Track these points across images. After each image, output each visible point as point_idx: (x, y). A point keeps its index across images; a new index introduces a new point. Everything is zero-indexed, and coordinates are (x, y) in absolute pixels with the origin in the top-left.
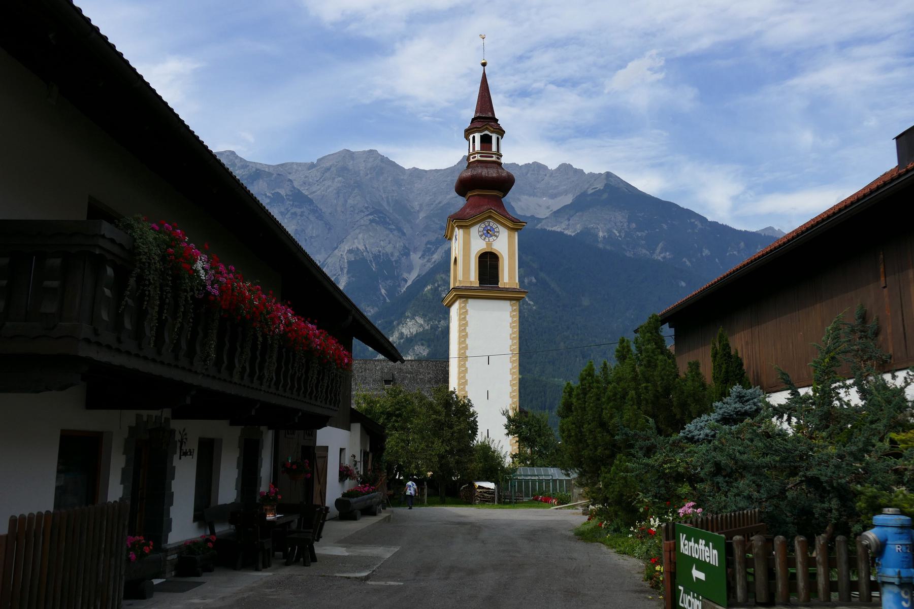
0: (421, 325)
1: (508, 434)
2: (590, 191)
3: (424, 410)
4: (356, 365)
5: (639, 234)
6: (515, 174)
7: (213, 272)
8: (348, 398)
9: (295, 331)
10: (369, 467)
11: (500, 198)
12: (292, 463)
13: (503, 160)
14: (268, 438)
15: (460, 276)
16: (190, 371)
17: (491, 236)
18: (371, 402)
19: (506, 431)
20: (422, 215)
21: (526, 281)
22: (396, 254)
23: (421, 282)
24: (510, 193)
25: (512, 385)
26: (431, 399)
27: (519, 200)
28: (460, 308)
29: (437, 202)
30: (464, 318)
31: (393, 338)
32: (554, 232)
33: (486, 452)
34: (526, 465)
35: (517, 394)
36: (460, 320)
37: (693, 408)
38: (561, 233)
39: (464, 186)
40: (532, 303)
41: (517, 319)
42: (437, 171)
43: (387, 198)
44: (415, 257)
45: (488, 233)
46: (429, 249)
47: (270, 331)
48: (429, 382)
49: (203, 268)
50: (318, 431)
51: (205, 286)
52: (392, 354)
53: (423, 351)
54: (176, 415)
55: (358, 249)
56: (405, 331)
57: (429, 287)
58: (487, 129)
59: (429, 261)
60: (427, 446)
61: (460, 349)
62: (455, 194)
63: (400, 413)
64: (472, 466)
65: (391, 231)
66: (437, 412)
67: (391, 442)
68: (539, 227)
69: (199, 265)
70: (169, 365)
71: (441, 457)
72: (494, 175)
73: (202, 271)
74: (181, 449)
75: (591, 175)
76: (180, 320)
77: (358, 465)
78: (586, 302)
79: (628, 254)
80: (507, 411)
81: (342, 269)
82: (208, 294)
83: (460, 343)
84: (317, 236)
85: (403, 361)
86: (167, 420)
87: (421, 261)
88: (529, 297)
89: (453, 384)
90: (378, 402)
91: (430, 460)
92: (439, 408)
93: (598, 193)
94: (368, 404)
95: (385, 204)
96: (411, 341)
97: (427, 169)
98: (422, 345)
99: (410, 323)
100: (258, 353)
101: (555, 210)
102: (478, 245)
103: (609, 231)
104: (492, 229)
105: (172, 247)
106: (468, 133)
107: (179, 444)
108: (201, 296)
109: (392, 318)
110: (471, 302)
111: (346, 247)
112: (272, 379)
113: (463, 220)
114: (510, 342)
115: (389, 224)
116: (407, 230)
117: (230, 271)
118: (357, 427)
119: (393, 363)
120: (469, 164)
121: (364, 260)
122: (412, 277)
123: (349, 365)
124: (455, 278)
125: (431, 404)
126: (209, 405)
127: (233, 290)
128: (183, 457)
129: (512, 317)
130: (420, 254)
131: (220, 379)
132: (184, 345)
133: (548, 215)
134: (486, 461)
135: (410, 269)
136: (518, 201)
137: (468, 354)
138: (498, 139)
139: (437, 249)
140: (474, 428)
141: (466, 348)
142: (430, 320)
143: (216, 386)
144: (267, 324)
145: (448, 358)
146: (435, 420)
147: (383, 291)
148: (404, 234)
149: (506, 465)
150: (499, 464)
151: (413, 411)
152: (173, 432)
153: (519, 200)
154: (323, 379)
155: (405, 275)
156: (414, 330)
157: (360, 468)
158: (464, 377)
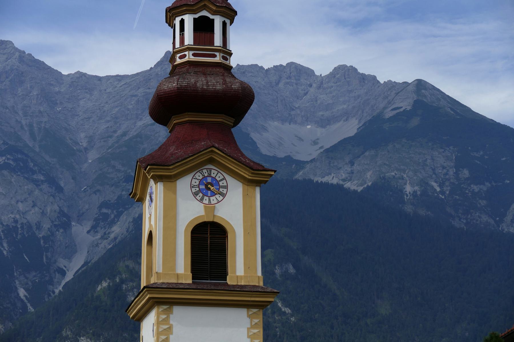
2: (389, 114)
5: (476, 188)
6: (255, 83)
11: (230, 127)
13: (233, 62)
15: (158, 266)
17: (214, 194)
20: (92, 156)
22: (46, 225)
23: (90, 274)
24: (248, 118)
27: (265, 129)
28: (159, 323)
29: (119, 132)
32: (327, 185)
38: (339, 187)
39: (166, 106)
40: (288, 311)
42: (119, 78)
43: (31, 126)
44: (80, 231)
45: (208, 189)
57: (105, 284)
58: (205, 8)
59: (104, 237)
62: (148, 120)
65: (37, 183)
68: (300, 176)
72: (219, 87)
75: (391, 85)
78: (384, 309)
79: (457, 224)
87: (90, 238)
88: (284, 301)
93: (403, 116)
95: (26, 137)
97: (102, 73)
101: (327, 146)
102: (191, 210)
103: (424, 183)
104: (215, 182)
106: (171, 14)
110: (178, 311)
113: (163, 166)
115: (34, 172)
116: (66, 181)
120: (175, 67)
122: (74, 267)
133: (315, 155)
135: (71, 251)
136: (263, 133)
138: (224, 24)
139: (118, 216)
147: (22, 293)
148: (60, 190)
153: (265, 129)
155: (62, 263)
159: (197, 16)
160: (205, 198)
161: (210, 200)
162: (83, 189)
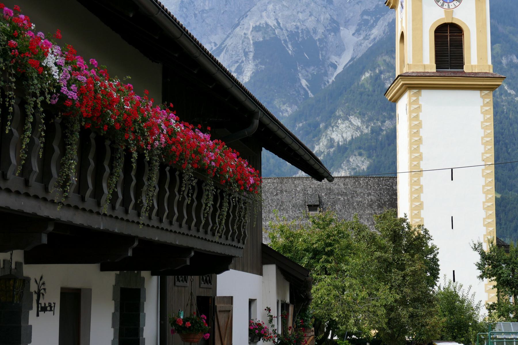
0: (358, 128)
1: (481, 277)
3: (364, 245)
4: (267, 185)
7: (69, 68)
8: (258, 231)
9: (182, 143)
10: (290, 323)
12: (185, 320)
14: (152, 286)
15: (409, 59)
16: (45, 199)
18: (291, 237)
19: (479, 273)
21: (504, 61)
22: (321, 30)
23: (356, 67)
25: (486, 209)
26: (373, 230)
28: (410, 103)
30: (417, 117)
31: (319, 148)
33: (452, 302)
34: (508, 319)
35: (493, 220)
36: (411, 119)
37: (445, 339)
40: (513, 92)
41: (490, 116)
44: (347, 34)
46: (367, 21)
47: (147, 143)
48: (371, 206)
49: (56, 64)
50: (218, 276)
51: (59, 88)
52: (316, 170)
53: (361, 163)
54: (30, 259)
55: (267, 24)
56: (336, 137)
57: (367, 75)
60: (370, 294)
61: (411, 160)
63: (329, 251)
64: (432, 321)
66: (382, 248)
67: (320, 290)
69: (50, 61)
70: (18, 193)
71: (390, 309)
73: (55, 69)
74: (38, 303)
76: (29, 133)
77: (275, 321)
80: (480, 245)
81: (246, 54)
82: (63, 98)
83: (411, 152)
84: (211, 9)
85: (331, 179)
86: (19, 265)
87: (355, 39)
88: (509, 84)
89: (404, 208)
90: (301, 235)
91: (374, 312)
92: (384, 242)
94: (287, 238)
96: (343, 150)
98: (360, 154)
99: (342, 126)
100: (133, 174)
105: (14, 37)
107: (35, 297)
108: (54, 102)
109: (318, 119)
111: (250, 23)
112: (153, 207)
114: (482, 149)
117: (92, 66)
118: (271, 270)
119: (319, 183)
121: (276, 39)
122: (343, 62)
123: (256, 187)
124: (402, 61)
125: (373, 237)
126: (70, 245)
127: (96, 92)
128: (41, 313)
129: (484, 113)
130: (353, 29)
131: (84, 210)
132: (36, 167)
134: (451, 313)
135: (340, 50)
137: (423, 167)
140: (433, 269)
141: (420, 158)
142: (371, 119)
143: (79, 219)
144: (143, 135)
145: (396, 173)
146: (378, 258)
147: (304, 83)
149: (480, 320)
150: (470, 318)
151: (348, 246)
152: (26, 281)
154: (221, 206)
155: (334, 59)
156: (348, 135)
157: (277, 326)
158: (418, 199)
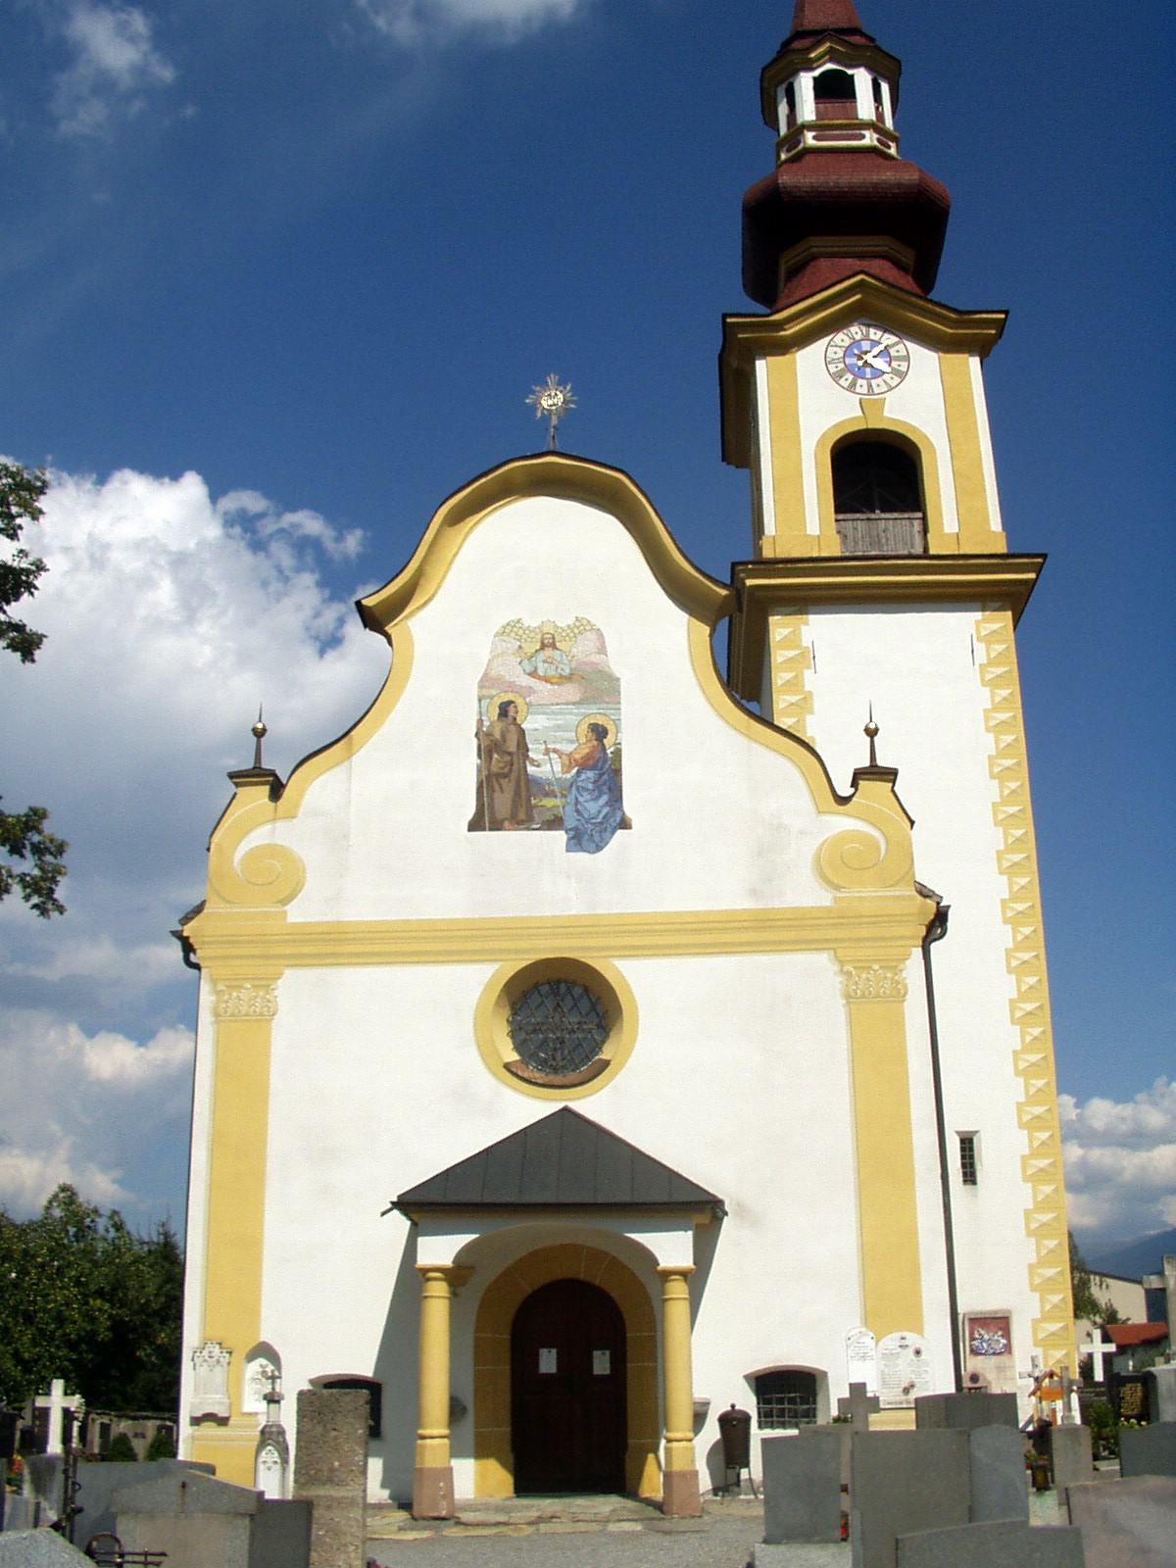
20: (102, 1336)
159: (817, 73)
160: (860, 382)
161: (870, 386)
162: (54, 1446)
